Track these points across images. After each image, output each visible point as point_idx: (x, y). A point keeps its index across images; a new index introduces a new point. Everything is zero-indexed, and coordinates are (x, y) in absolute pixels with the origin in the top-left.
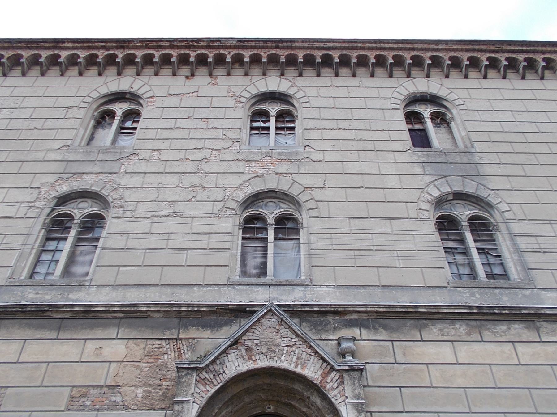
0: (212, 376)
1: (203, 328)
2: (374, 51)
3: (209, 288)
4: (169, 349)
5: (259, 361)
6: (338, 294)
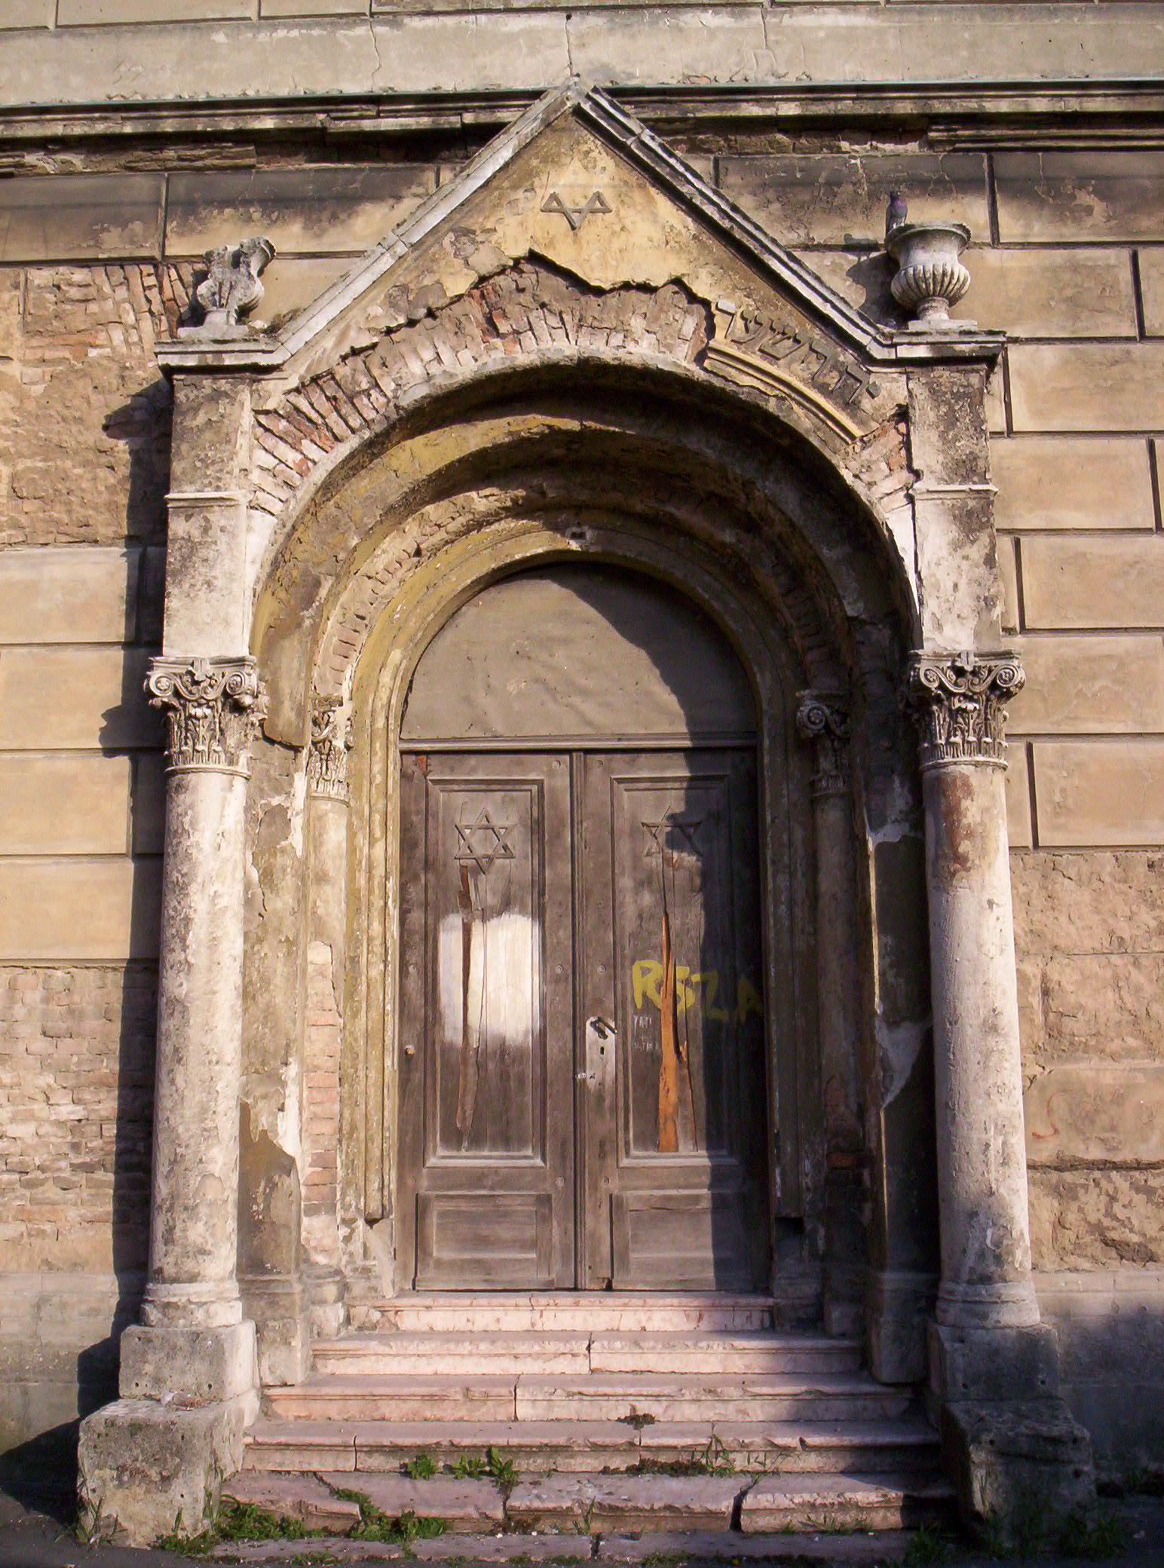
0: (324, 406)
1: (266, 213)
2: (585, 1299)
3: (281, 33)
4: (128, 306)
5: (528, 339)
6: (892, 43)
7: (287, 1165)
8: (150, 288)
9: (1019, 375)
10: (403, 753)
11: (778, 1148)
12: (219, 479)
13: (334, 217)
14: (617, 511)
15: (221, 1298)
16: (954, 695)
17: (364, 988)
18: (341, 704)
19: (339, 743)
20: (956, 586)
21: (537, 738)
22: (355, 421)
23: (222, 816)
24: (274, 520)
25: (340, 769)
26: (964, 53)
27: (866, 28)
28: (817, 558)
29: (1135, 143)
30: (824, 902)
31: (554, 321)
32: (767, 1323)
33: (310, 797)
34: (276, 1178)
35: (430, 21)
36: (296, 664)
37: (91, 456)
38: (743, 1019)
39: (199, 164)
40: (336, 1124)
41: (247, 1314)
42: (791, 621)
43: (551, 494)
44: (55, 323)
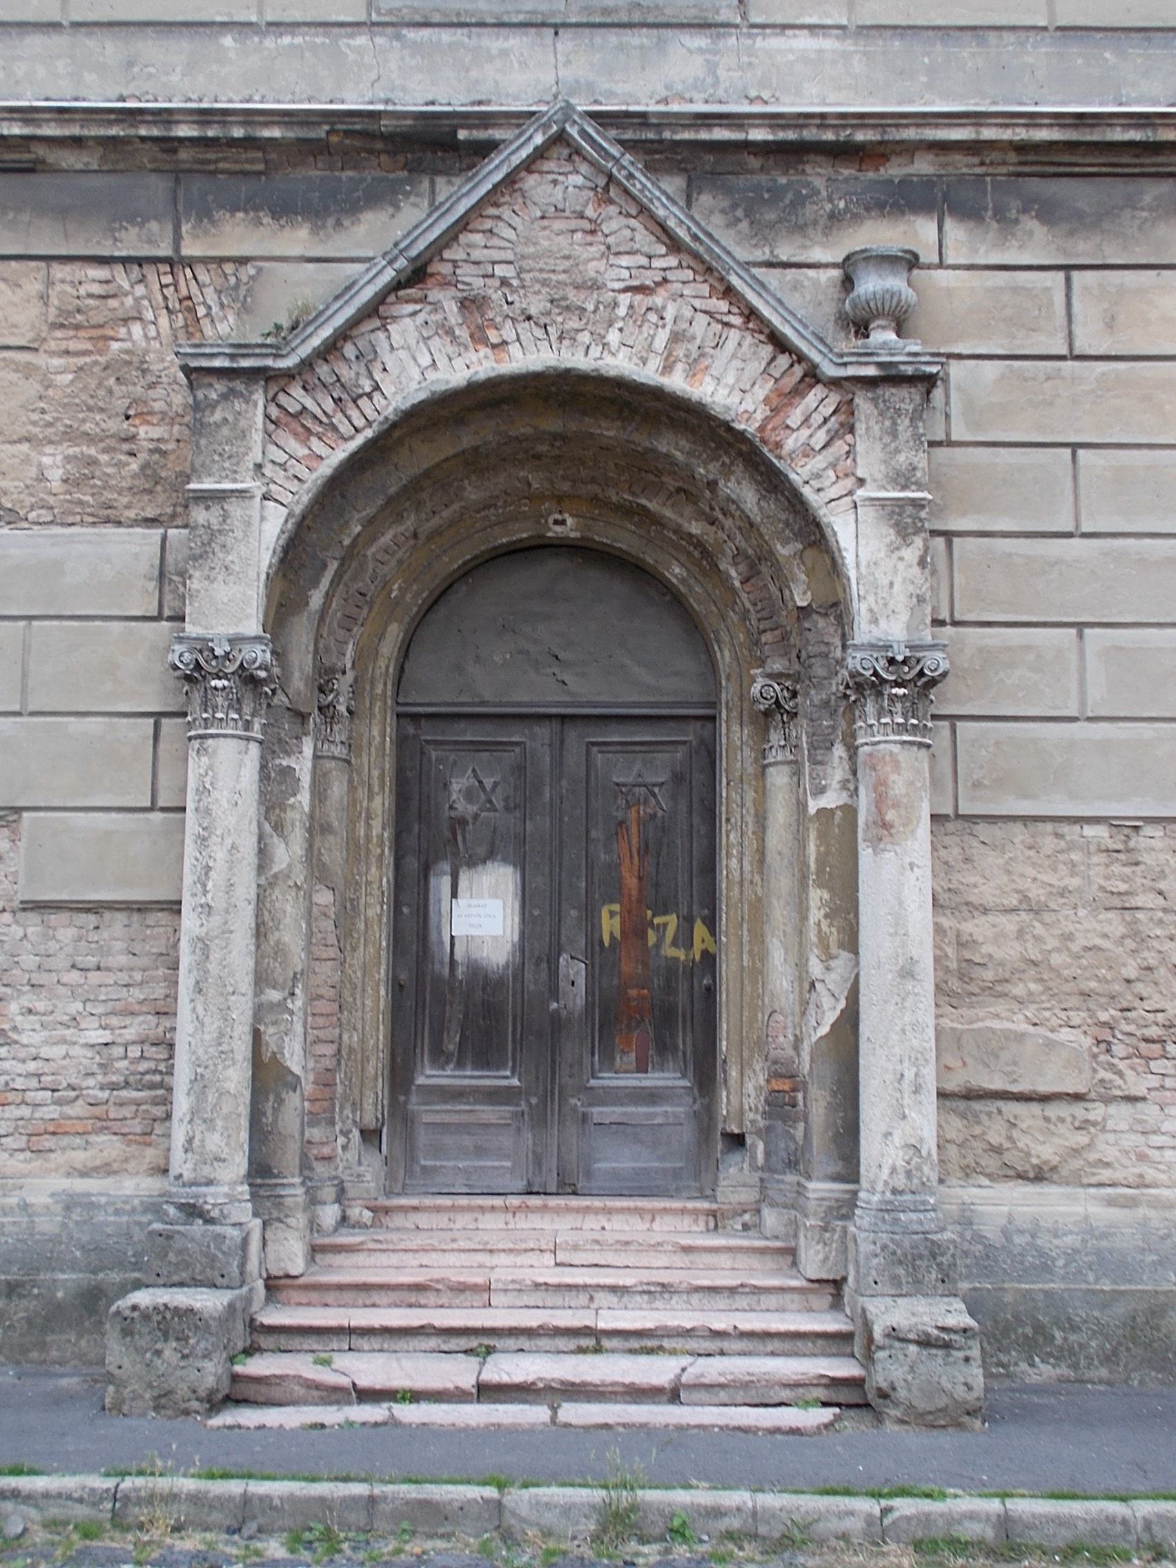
0: (329, 405)
1: (275, 216)
3: (286, 40)
4: (146, 303)
5: (514, 349)
6: (858, 65)
7: (294, 1083)
8: (167, 286)
9: (959, 389)
10: (399, 716)
11: (725, 1072)
12: (235, 472)
13: (339, 224)
14: (594, 500)
15: (233, 1199)
16: (886, 681)
17: (362, 926)
18: (344, 673)
19: (342, 708)
20: (891, 584)
21: (519, 704)
22: (360, 422)
23: (239, 776)
24: (285, 511)
25: (340, 732)
26: (924, 79)
27: (833, 51)
28: (771, 553)
29: (1077, 169)
30: (771, 856)
31: (539, 333)
32: (712, 1225)
33: (316, 757)
34: (284, 1095)
35: (426, 33)
36: (304, 640)
37: (112, 442)
38: (697, 958)
39: (212, 167)
40: (335, 1046)
41: (256, 1214)
42: (748, 605)
43: (535, 485)
44: (79, 317)
